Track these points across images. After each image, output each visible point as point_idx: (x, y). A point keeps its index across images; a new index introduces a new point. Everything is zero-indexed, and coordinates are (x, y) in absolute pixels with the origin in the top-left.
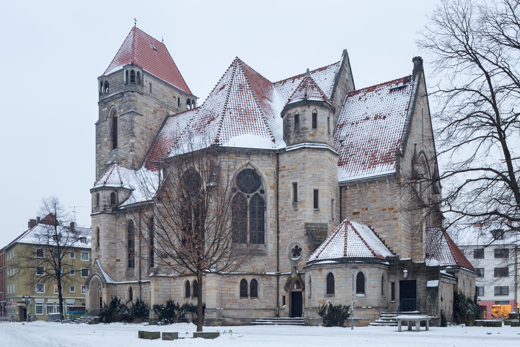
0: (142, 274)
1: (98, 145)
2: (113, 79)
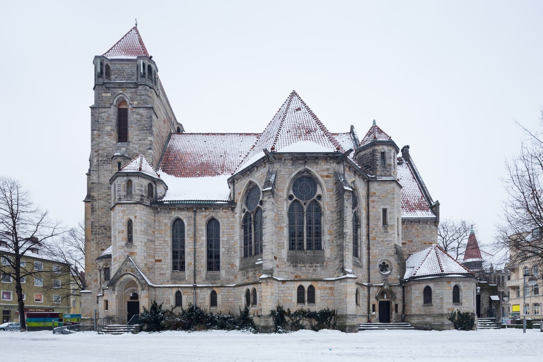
0: (198, 277)
1: (95, 132)
2: (118, 66)
